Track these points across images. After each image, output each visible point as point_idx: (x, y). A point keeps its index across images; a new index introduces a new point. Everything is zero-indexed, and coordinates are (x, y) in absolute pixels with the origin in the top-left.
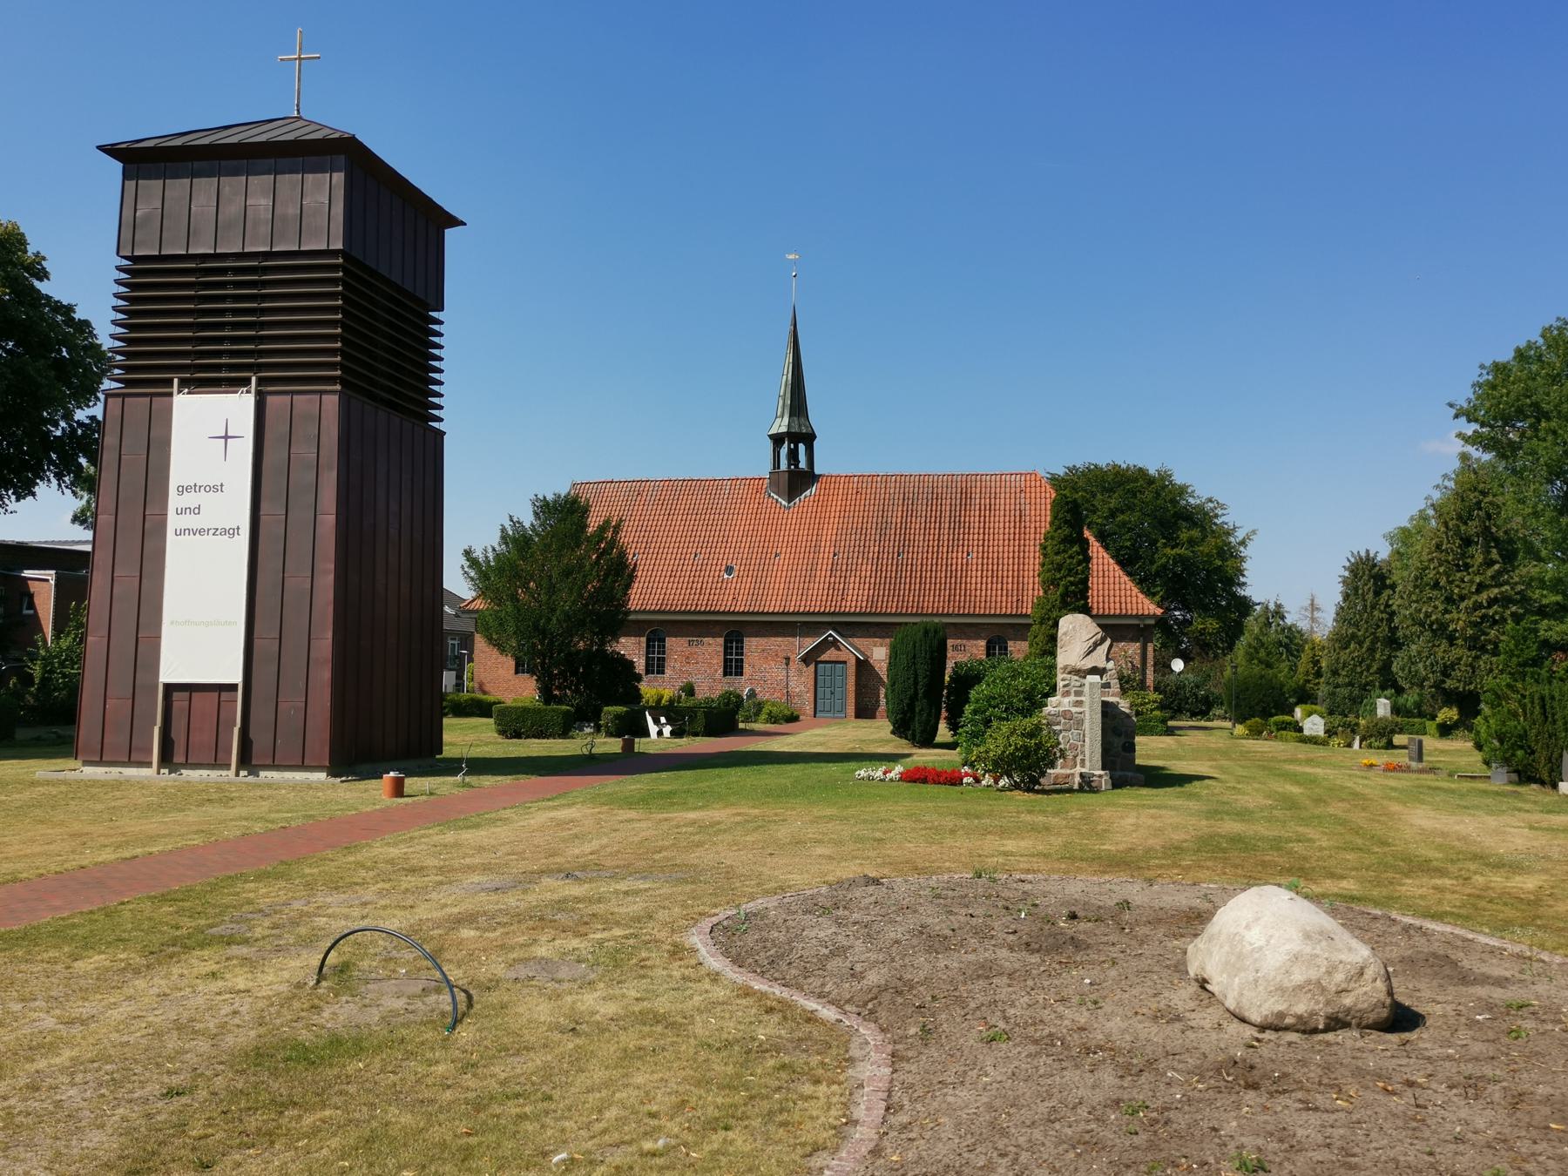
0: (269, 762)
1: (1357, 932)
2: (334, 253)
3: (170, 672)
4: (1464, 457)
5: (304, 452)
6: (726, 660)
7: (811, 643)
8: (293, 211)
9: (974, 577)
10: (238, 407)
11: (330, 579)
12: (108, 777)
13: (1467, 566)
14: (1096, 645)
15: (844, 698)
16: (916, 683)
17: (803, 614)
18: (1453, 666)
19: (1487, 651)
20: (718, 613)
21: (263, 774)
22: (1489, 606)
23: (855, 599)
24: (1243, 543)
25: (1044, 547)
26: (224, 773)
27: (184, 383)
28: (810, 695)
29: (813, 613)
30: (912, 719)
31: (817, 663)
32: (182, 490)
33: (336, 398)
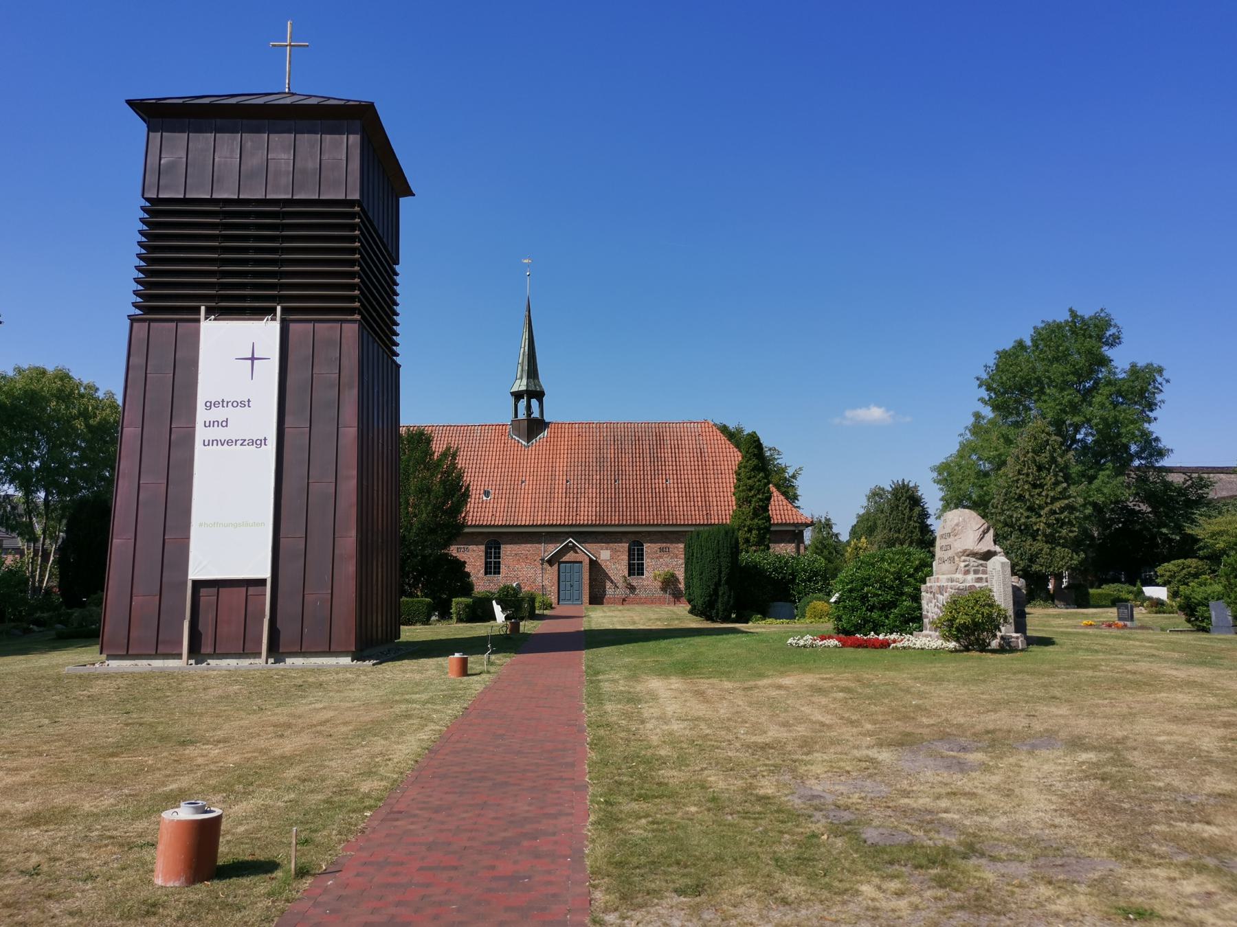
0: (297, 649)
1: (893, 748)
2: (352, 203)
3: (197, 571)
4: (977, 416)
5: (326, 373)
6: (486, 563)
7: (552, 549)
8: (312, 165)
9: (673, 497)
10: (263, 334)
11: (353, 483)
12: (136, 670)
13: (1042, 486)
14: (985, 533)
15: (580, 590)
16: (720, 572)
17: (548, 526)
18: (1037, 554)
19: (1059, 544)
20: (482, 526)
21: (289, 661)
22: (1062, 512)
23: (586, 515)
24: (794, 476)
25: (738, 474)
26: (257, 661)
27: (210, 311)
28: (555, 588)
29: (556, 525)
30: (716, 601)
31: (560, 563)
32: (209, 405)
33: (356, 326)
